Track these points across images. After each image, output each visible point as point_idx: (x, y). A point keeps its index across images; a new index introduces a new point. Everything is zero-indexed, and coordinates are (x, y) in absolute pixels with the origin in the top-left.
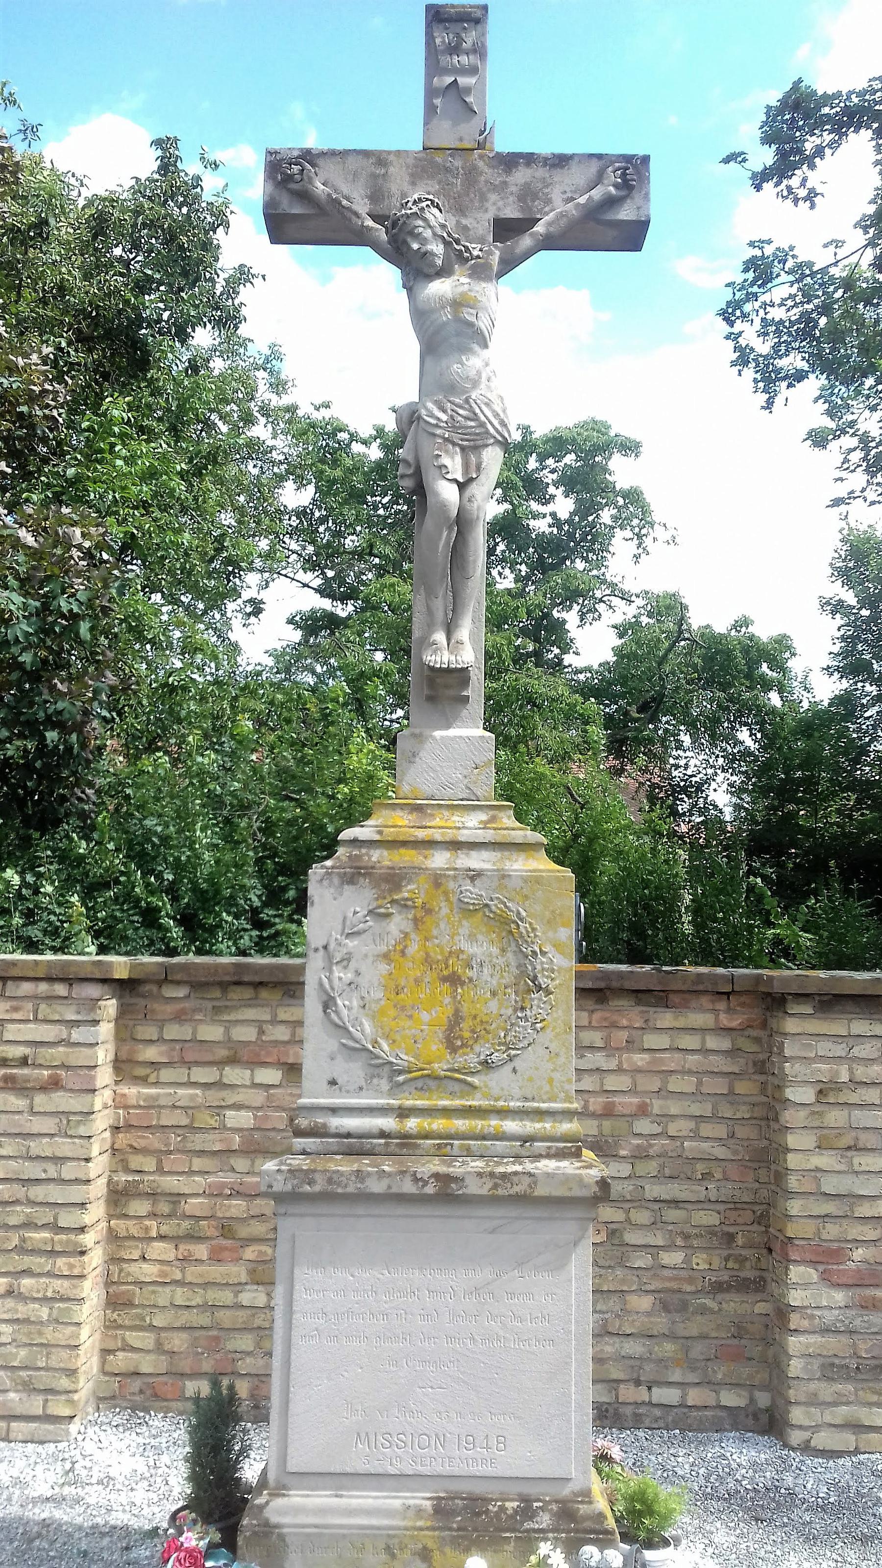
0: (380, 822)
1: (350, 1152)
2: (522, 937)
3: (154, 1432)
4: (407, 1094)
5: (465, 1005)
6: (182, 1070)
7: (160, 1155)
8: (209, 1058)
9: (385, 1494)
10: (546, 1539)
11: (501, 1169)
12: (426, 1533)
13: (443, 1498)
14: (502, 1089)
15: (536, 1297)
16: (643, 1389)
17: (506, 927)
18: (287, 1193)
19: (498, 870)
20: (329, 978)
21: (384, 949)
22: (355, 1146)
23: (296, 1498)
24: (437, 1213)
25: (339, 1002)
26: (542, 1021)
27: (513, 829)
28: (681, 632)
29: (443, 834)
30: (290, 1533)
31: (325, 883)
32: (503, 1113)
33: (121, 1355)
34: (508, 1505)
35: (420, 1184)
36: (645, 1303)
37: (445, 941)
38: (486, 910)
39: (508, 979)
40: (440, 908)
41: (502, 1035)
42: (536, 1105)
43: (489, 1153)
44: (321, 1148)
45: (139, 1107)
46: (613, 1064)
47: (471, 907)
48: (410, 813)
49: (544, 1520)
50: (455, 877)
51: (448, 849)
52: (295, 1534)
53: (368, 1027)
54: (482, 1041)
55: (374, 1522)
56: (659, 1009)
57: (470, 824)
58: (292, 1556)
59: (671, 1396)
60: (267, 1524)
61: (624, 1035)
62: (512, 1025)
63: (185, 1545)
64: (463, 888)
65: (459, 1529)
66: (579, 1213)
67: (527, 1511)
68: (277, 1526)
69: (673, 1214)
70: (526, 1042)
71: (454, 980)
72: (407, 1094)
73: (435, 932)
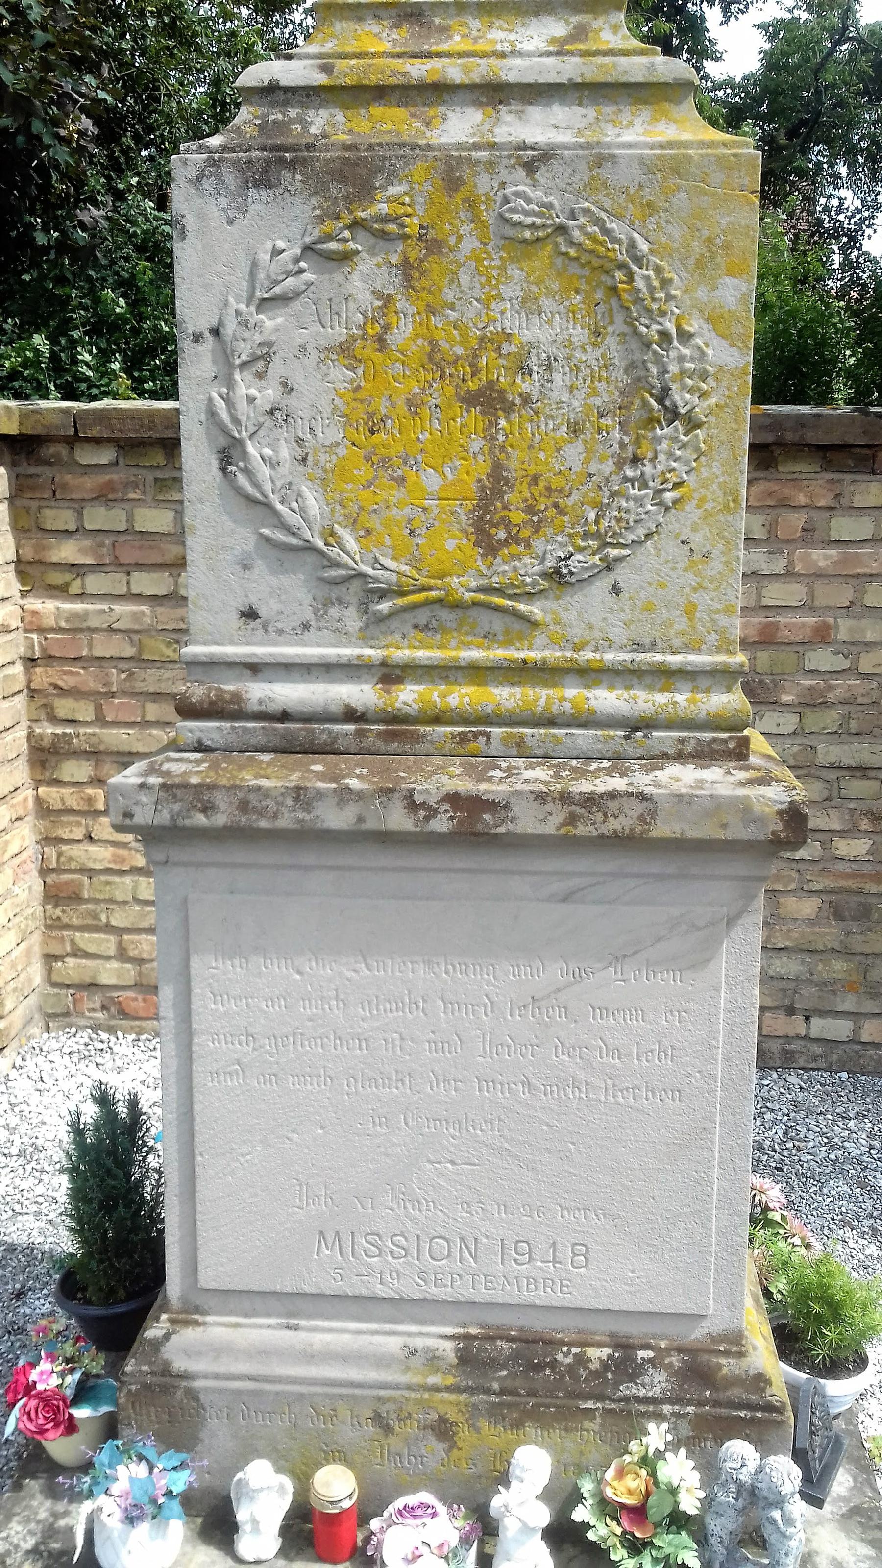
0: (329, 47)
1: (286, 748)
2: (638, 300)
3: (119, 1063)
4: (398, 636)
5: (515, 454)
6: (118, 575)
7: (100, 698)
8: (156, 558)
9: (374, 1326)
10: (659, 1417)
11: (584, 786)
12: (446, 1395)
13: (475, 1337)
14: (591, 627)
15: (651, 1016)
16: (799, 1019)
17: (605, 280)
18: (163, 828)
19: (588, 146)
20: (227, 400)
21: (340, 333)
22: (296, 736)
23: (217, 1329)
24: (459, 865)
25: (251, 449)
26: (677, 485)
27: (625, 53)
28: (845, 28)
29: (466, 70)
30: (206, 1389)
31: (208, 184)
32: (590, 675)
33: (71, 961)
34: (593, 1353)
35: (422, 813)
36: (808, 907)
37: (471, 314)
38: (560, 239)
39: (606, 395)
40: (460, 238)
41: (592, 516)
42: (659, 657)
43: (561, 750)
44: (232, 739)
45: (60, 630)
46: (779, 565)
47: (527, 234)
48: (397, 26)
49: (657, 1382)
50: (491, 165)
51: (477, 104)
52: (214, 1390)
53: (313, 503)
54: (549, 531)
55: (354, 1374)
56: (858, 477)
57: (527, 46)
58: (213, 1423)
59: (840, 1029)
60: (166, 1371)
61: (798, 520)
62: (613, 494)
63: (40, 1387)
64: (510, 190)
65: (502, 1392)
66: (741, 867)
67: (625, 1363)
68: (185, 1376)
69: (857, 787)
70: (641, 531)
71: (490, 401)
72: (398, 636)
73: (449, 295)
